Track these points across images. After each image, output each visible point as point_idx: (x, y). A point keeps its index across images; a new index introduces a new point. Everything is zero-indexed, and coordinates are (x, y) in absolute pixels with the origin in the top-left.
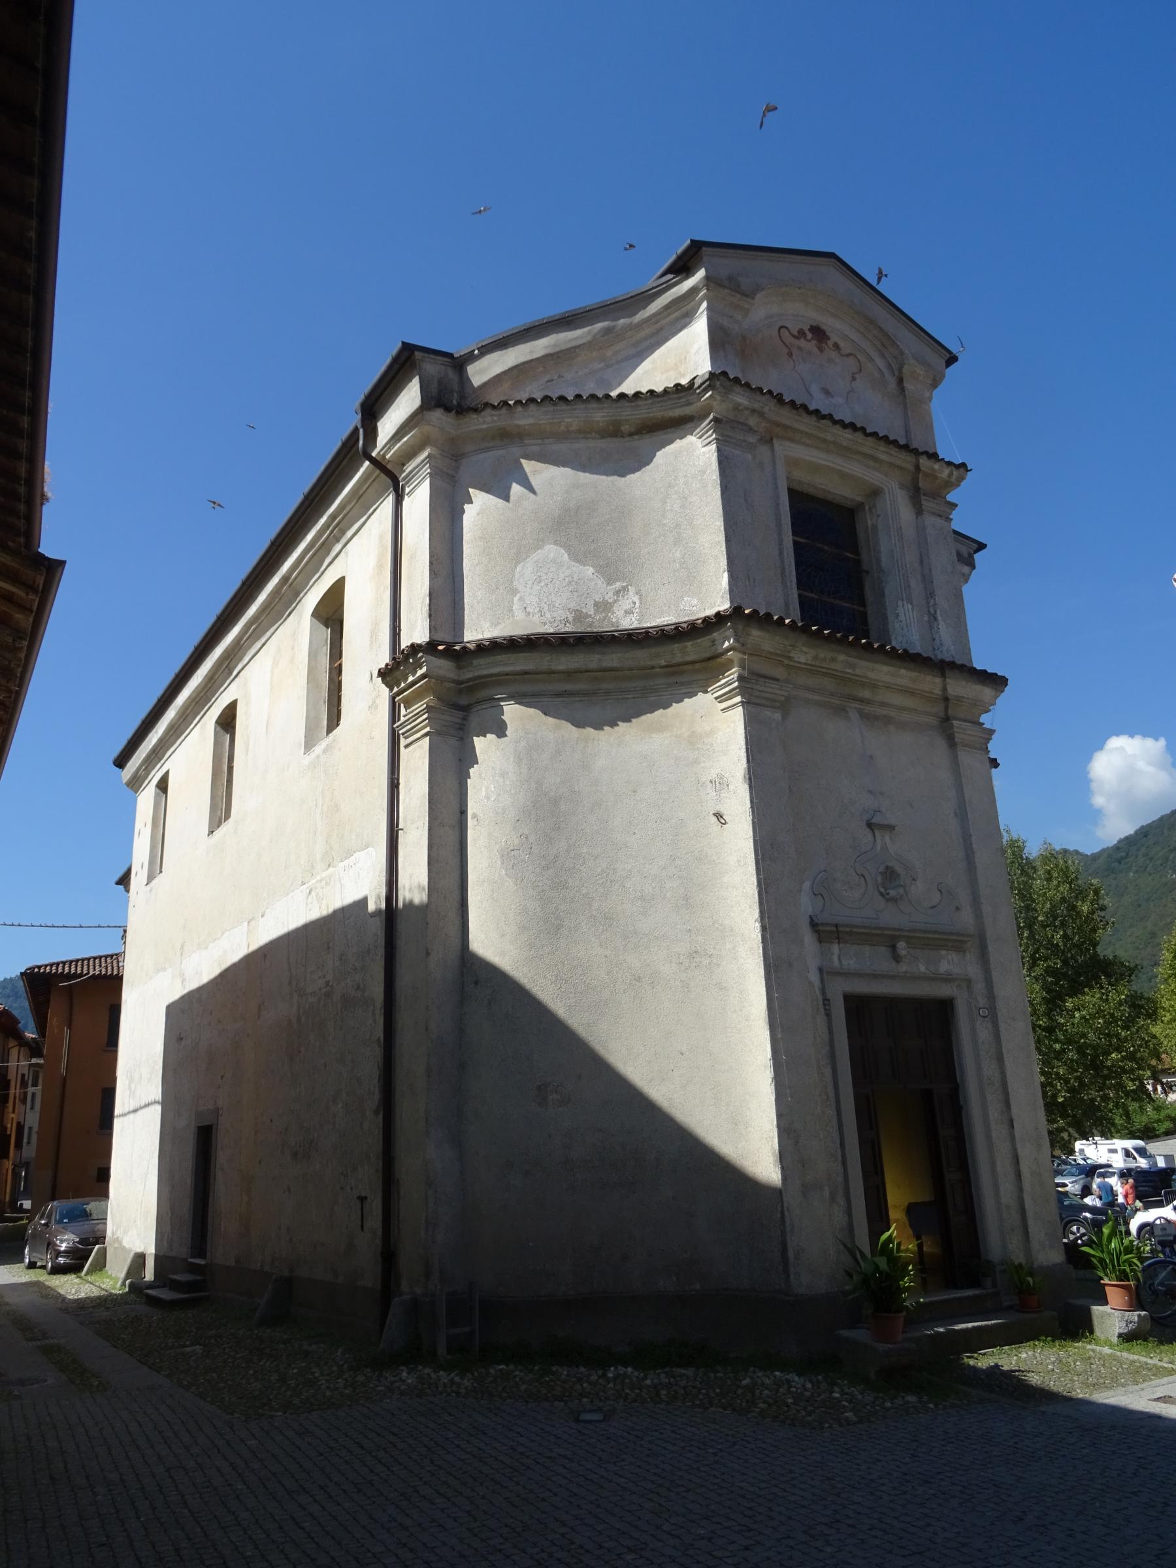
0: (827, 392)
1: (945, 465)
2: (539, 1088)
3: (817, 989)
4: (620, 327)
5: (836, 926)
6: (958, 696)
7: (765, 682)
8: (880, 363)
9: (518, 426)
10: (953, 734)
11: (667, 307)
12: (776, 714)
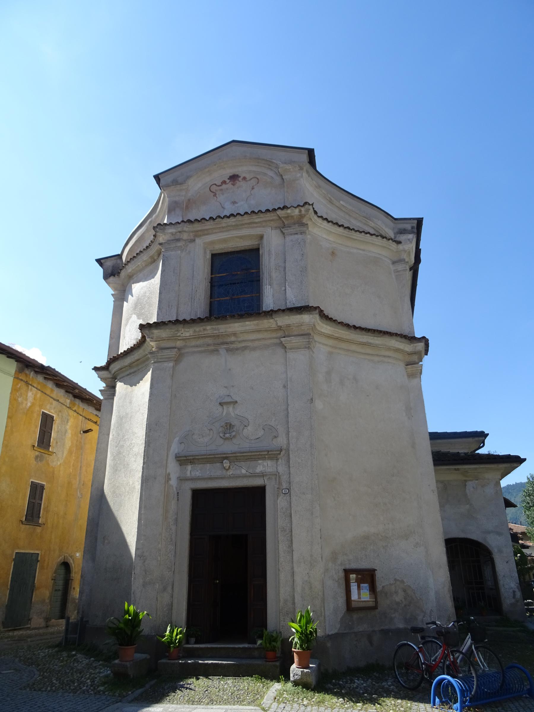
8: (271, 173)
9: (130, 272)
11: (162, 203)
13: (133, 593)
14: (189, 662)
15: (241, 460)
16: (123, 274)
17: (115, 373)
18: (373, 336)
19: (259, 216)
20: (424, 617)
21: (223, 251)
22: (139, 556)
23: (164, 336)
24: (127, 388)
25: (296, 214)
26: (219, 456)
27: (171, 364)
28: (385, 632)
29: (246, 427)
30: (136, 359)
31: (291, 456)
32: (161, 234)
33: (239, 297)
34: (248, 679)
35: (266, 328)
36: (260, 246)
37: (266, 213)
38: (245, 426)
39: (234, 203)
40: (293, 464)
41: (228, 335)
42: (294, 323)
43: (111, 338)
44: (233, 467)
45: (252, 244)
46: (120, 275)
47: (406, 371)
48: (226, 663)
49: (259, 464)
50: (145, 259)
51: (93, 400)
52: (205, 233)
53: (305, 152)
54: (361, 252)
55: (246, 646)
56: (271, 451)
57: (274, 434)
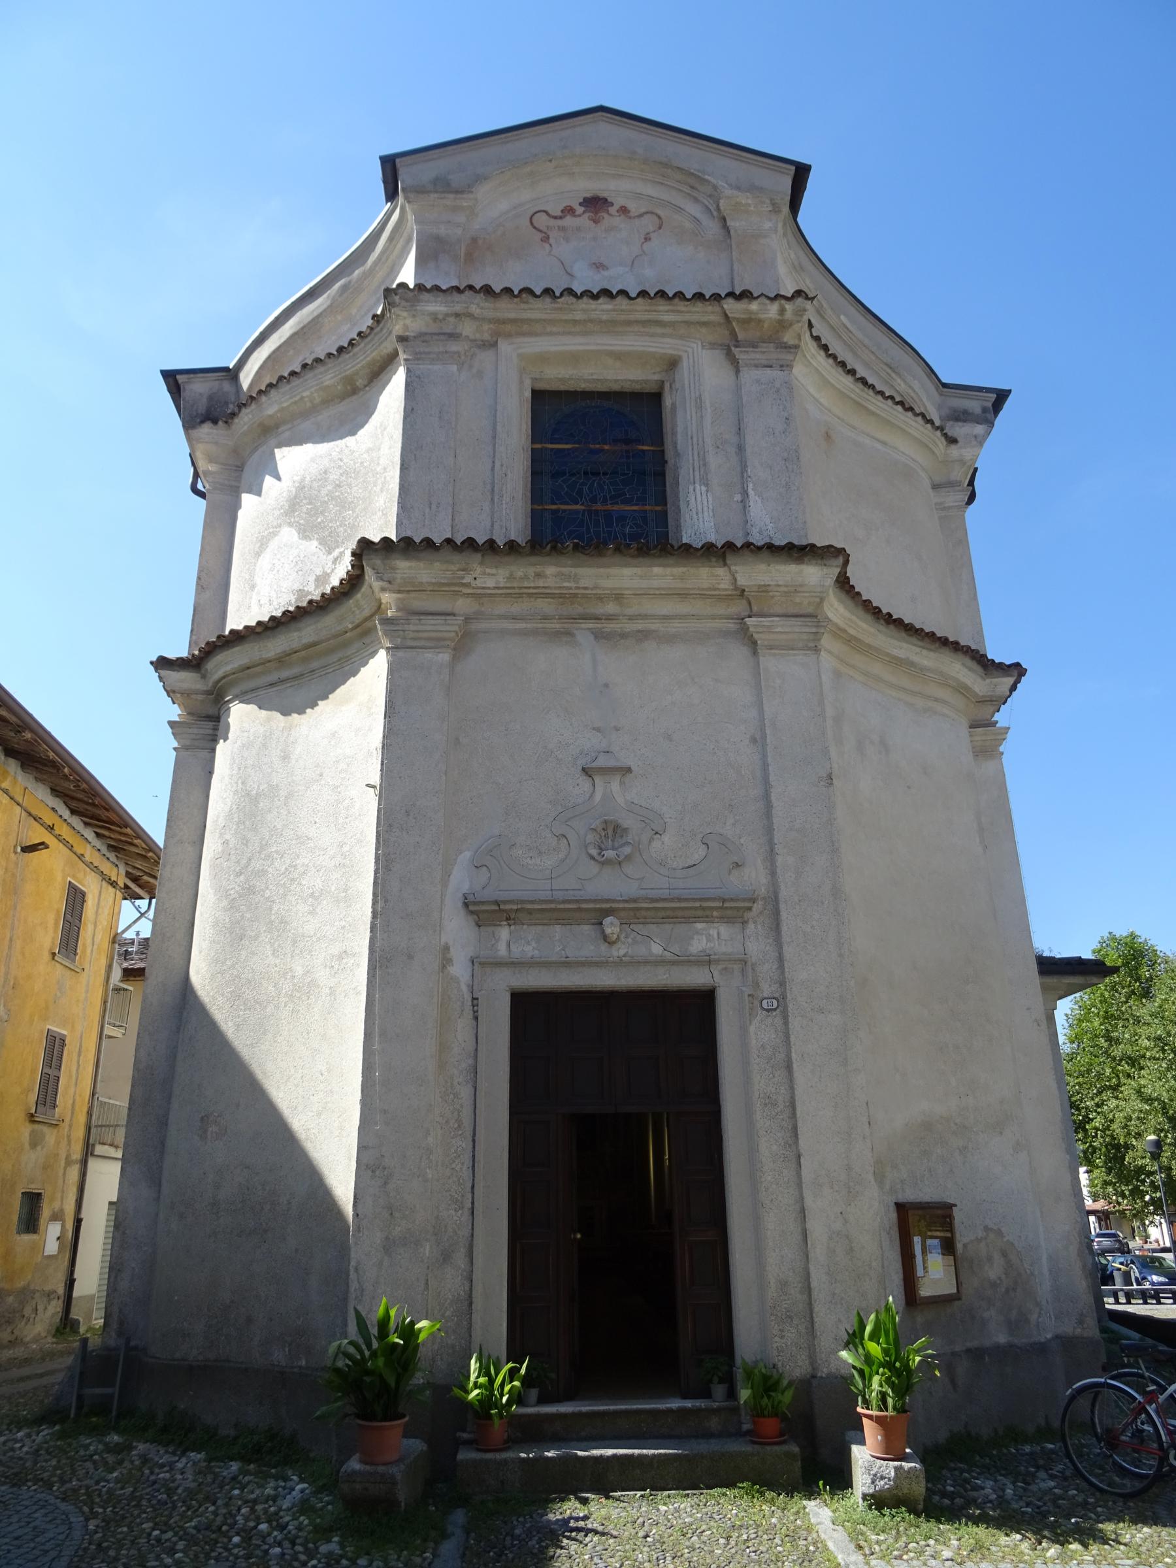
0: (599, 266)
4: (354, 280)
5: (497, 903)
6: (760, 586)
7: (420, 620)
8: (693, 209)
9: (270, 416)
11: (391, 239)
13: (356, 1270)
14: (550, 1454)
15: (648, 920)
16: (246, 419)
17: (224, 677)
18: (920, 647)
19: (675, 308)
20: (1039, 1317)
21: (562, 388)
22: (367, 1167)
23: (424, 580)
24: (269, 719)
25: (771, 315)
26: (591, 906)
27: (445, 657)
28: (976, 1354)
29: (658, 836)
30: (305, 641)
31: (784, 915)
32: (405, 314)
33: (609, 507)
34: (725, 1495)
35: (703, 589)
36: (667, 386)
37: (693, 301)
38: (657, 833)
39: (597, 267)
40: (791, 937)
41: (600, 598)
42: (780, 583)
43: (201, 586)
44: (626, 937)
45: (645, 378)
46: (236, 420)
47: (971, 742)
48: (654, 1455)
49: (697, 933)
50: (327, 383)
51: (63, 766)
52: (522, 329)
53: (790, 170)
54: (879, 446)
55: (675, 1404)
56: (732, 900)
57: (736, 859)
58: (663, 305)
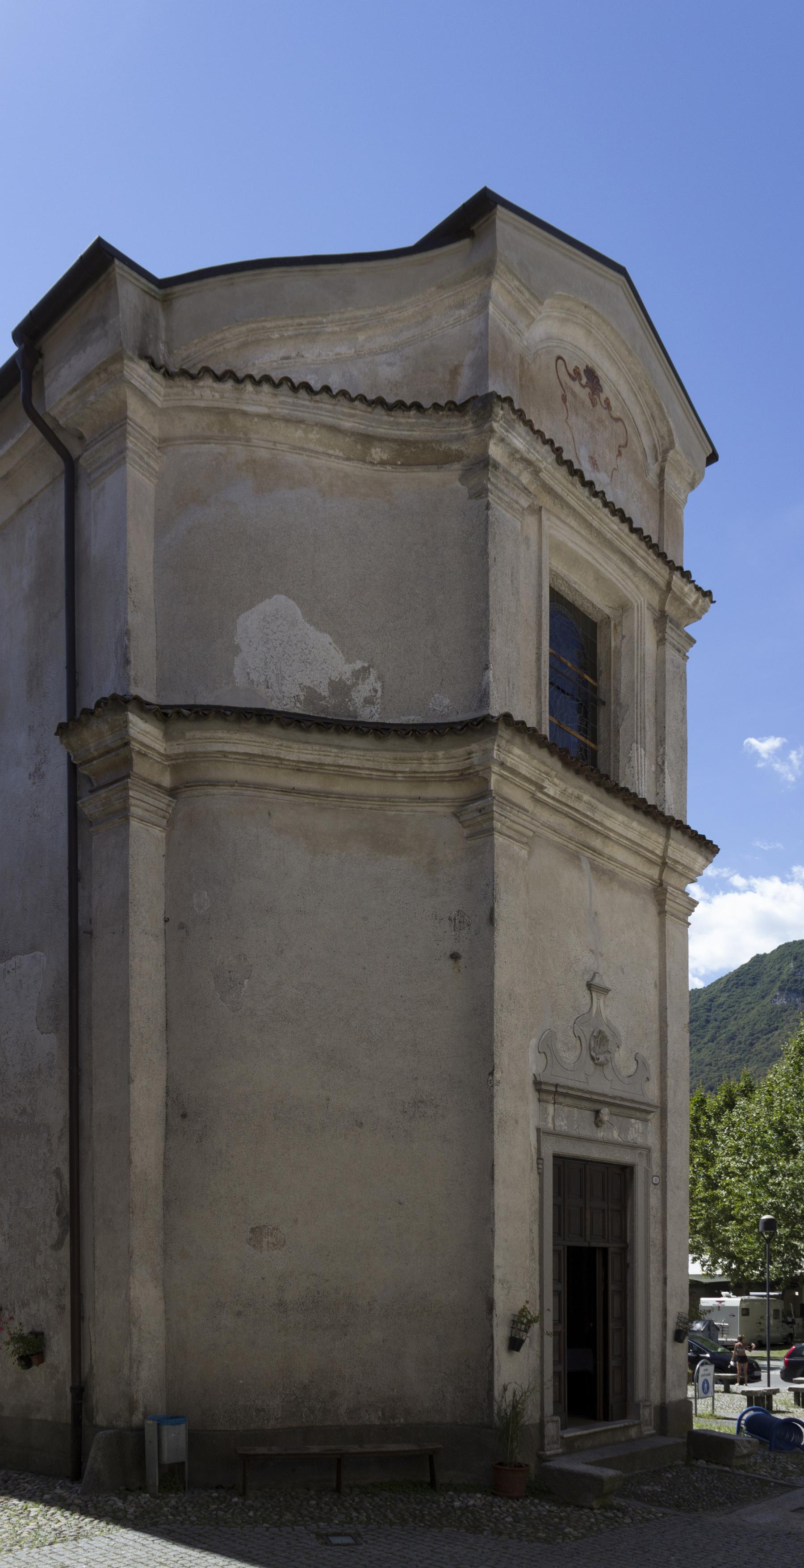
1: (694, 590)
2: (253, 1230)
3: (533, 1149)
10: (664, 900)
12: (523, 851)
58: (643, 549)
